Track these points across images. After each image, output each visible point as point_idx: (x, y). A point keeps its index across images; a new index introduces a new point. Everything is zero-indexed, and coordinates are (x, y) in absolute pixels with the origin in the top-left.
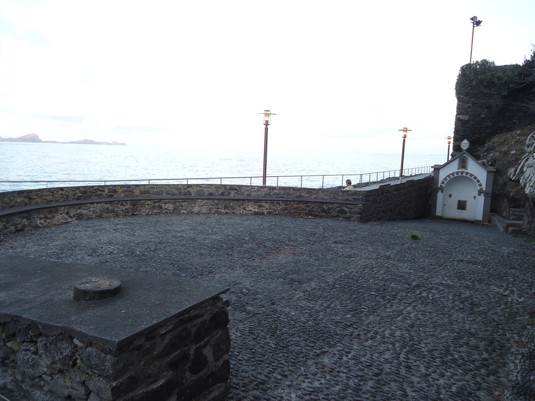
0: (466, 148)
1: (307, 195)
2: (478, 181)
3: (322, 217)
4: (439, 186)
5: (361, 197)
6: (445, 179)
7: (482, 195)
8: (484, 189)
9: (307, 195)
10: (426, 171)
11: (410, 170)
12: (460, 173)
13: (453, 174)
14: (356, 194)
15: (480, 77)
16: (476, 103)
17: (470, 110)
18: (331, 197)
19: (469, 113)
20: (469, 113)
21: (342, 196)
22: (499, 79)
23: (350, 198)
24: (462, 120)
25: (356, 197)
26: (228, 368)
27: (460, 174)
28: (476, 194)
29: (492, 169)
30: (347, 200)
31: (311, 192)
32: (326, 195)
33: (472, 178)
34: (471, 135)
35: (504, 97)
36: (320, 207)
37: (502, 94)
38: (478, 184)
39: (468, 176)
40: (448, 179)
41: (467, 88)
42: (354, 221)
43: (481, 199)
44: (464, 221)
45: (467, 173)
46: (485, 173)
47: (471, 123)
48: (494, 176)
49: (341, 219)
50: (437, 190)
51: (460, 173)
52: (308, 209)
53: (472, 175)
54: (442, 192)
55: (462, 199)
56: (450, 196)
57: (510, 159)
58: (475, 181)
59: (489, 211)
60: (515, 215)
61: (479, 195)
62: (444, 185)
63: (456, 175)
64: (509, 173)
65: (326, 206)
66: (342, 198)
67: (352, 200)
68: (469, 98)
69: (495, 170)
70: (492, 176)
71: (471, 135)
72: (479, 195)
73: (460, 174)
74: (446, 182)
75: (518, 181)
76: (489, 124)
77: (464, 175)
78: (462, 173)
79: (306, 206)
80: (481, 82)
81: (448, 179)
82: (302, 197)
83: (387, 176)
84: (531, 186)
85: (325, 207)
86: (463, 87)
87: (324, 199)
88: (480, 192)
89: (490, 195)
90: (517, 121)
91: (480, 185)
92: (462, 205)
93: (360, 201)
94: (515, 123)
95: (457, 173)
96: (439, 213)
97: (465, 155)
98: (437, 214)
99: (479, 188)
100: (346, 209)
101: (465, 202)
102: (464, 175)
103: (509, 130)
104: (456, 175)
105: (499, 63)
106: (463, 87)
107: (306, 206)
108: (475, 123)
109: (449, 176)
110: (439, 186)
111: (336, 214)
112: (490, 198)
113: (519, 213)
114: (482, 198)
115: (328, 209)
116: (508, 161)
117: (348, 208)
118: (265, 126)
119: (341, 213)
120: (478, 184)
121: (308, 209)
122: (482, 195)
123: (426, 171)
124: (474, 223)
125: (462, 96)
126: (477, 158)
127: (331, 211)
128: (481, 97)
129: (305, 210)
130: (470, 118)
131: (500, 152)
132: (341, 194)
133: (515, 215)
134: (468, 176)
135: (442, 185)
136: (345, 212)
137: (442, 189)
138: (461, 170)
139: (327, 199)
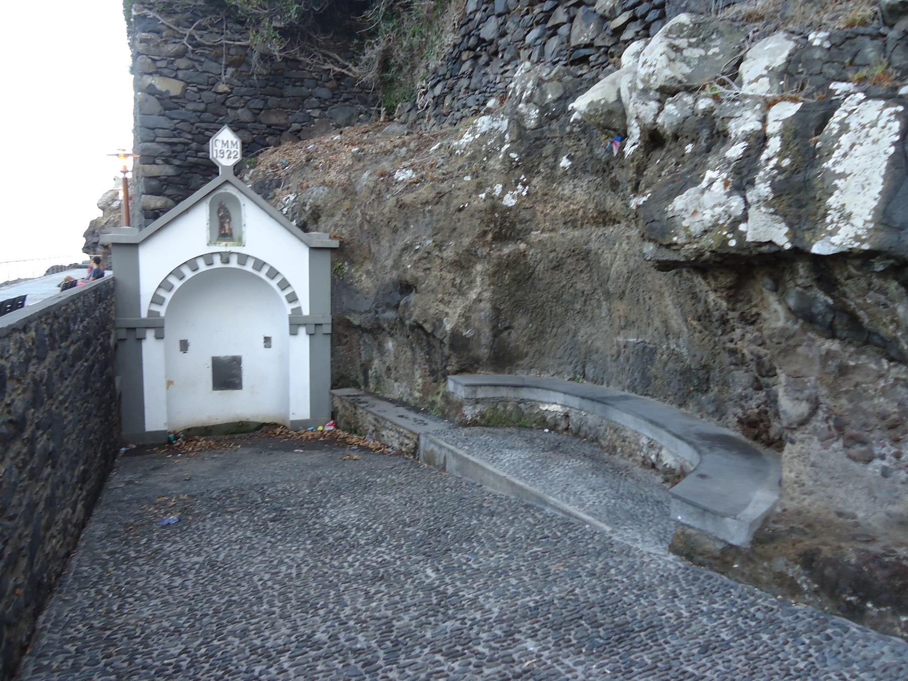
0: (231, 162)
2: (284, 285)
4: (144, 314)
6: (165, 285)
7: (302, 331)
8: (306, 312)
13: (192, 264)
17: (182, 63)
19: (181, 74)
20: (181, 74)
24: (161, 93)
28: (279, 328)
29: (321, 238)
33: (262, 274)
38: (283, 295)
39: (249, 267)
40: (177, 284)
45: (243, 259)
46: (302, 255)
47: (190, 106)
48: (333, 264)
50: (136, 333)
53: (259, 264)
54: (159, 337)
55: (226, 351)
56: (184, 346)
57: (408, 198)
58: (274, 283)
59: (329, 385)
60: (477, 401)
61: (293, 333)
62: (162, 310)
63: (203, 267)
69: (335, 244)
70: (326, 260)
72: (293, 333)
73: (218, 263)
74: (168, 296)
77: (234, 263)
81: (177, 284)
89: (328, 329)
90: (316, 113)
91: (292, 298)
92: (227, 374)
94: (311, 118)
95: (208, 258)
99: (289, 308)
101: (236, 362)
103: (297, 136)
108: (202, 107)
109: (177, 272)
110: (144, 314)
112: (329, 338)
113: (490, 393)
114: (303, 341)
116: (402, 206)
120: (283, 295)
122: (302, 331)
126: (266, 191)
128: (212, 25)
130: (185, 90)
133: (477, 401)
134: (249, 267)
135: (155, 308)
137: (158, 327)
138: (222, 247)
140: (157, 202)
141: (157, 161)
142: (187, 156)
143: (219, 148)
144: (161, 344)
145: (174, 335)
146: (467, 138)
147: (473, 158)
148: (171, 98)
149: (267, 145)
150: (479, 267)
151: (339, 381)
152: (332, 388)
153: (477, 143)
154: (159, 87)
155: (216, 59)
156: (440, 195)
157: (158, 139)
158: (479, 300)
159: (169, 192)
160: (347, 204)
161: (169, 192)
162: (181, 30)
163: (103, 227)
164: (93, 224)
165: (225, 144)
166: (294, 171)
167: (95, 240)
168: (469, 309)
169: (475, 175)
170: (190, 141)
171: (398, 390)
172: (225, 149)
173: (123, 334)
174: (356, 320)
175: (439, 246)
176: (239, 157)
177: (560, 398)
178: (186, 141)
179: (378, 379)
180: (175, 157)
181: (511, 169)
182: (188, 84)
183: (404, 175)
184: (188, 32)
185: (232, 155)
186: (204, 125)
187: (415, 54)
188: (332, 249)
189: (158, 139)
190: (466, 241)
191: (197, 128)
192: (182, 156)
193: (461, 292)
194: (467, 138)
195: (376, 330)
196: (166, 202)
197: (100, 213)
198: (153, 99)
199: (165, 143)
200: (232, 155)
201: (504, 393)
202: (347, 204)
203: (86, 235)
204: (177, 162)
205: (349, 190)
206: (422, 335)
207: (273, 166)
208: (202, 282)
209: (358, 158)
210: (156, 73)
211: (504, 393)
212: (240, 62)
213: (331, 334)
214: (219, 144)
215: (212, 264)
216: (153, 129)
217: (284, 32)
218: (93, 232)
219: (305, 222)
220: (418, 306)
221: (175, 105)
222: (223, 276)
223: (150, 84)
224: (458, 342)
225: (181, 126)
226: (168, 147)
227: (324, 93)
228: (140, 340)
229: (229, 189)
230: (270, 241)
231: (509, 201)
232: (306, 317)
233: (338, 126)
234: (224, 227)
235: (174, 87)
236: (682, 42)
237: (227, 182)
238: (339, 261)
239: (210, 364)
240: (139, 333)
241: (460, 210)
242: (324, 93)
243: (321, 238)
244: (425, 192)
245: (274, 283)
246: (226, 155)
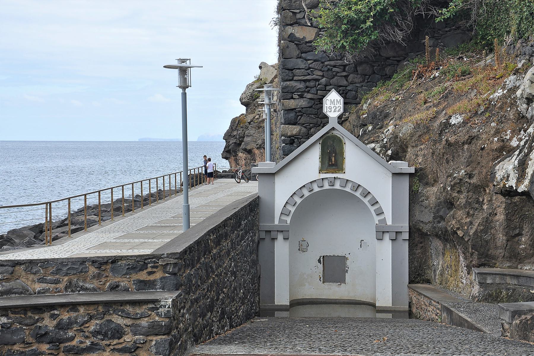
8: (389, 222)
10: (167, 185)
11: (146, 185)
14: (144, 267)
21: (98, 277)
24: (299, 40)
25: (143, 276)
27: (327, 186)
28: (370, 236)
33: (358, 194)
39: (348, 189)
50: (271, 235)
58: (372, 209)
64: (499, 175)
69: (412, 170)
74: (293, 209)
83: (77, 205)
85: (48, 323)
91: (380, 213)
92: (334, 268)
96: (282, 298)
98: (276, 303)
99: (377, 219)
101: (343, 259)
102: (337, 186)
110: (277, 222)
111: (88, 343)
112: (407, 244)
114: (387, 245)
115: (60, 326)
117: (128, 316)
118: (181, 91)
122: (387, 237)
123: (167, 185)
140: (294, 130)
141: (294, 96)
142: (317, 90)
143: (328, 106)
144: (287, 244)
148: (307, 42)
152: (409, 283)
154: (297, 35)
157: (295, 78)
165: (332, 102)
169: (500, 122)
170: (320, 77)
172: (332, 106)
173: (263, 235)
176: (342, 111)
178: (317, 77)
180: (308, 92)
181: (518, 119)
185: (337, 110)
186: (332, 63)
188: (411, 175)
189: (295, 78)
191: (327, 65)
192: (313, 90)
196: (300, 130)
199: (300, 80)
200: (337, 110)
204: (309, 96)
210: (296, 23)
213: (409, 240)
214: (328, 103)
215: (333, 185)
216: (292, 70)
221: (310, 49)
223: (291, 34)
226: (303, 83)
228: (274, 239)
230: (361, 166)
232: (390, 226)
234: (332, 159)
237: (333, 129)
240: (273, 234)
241: (482, 149)
246: (333, 110)
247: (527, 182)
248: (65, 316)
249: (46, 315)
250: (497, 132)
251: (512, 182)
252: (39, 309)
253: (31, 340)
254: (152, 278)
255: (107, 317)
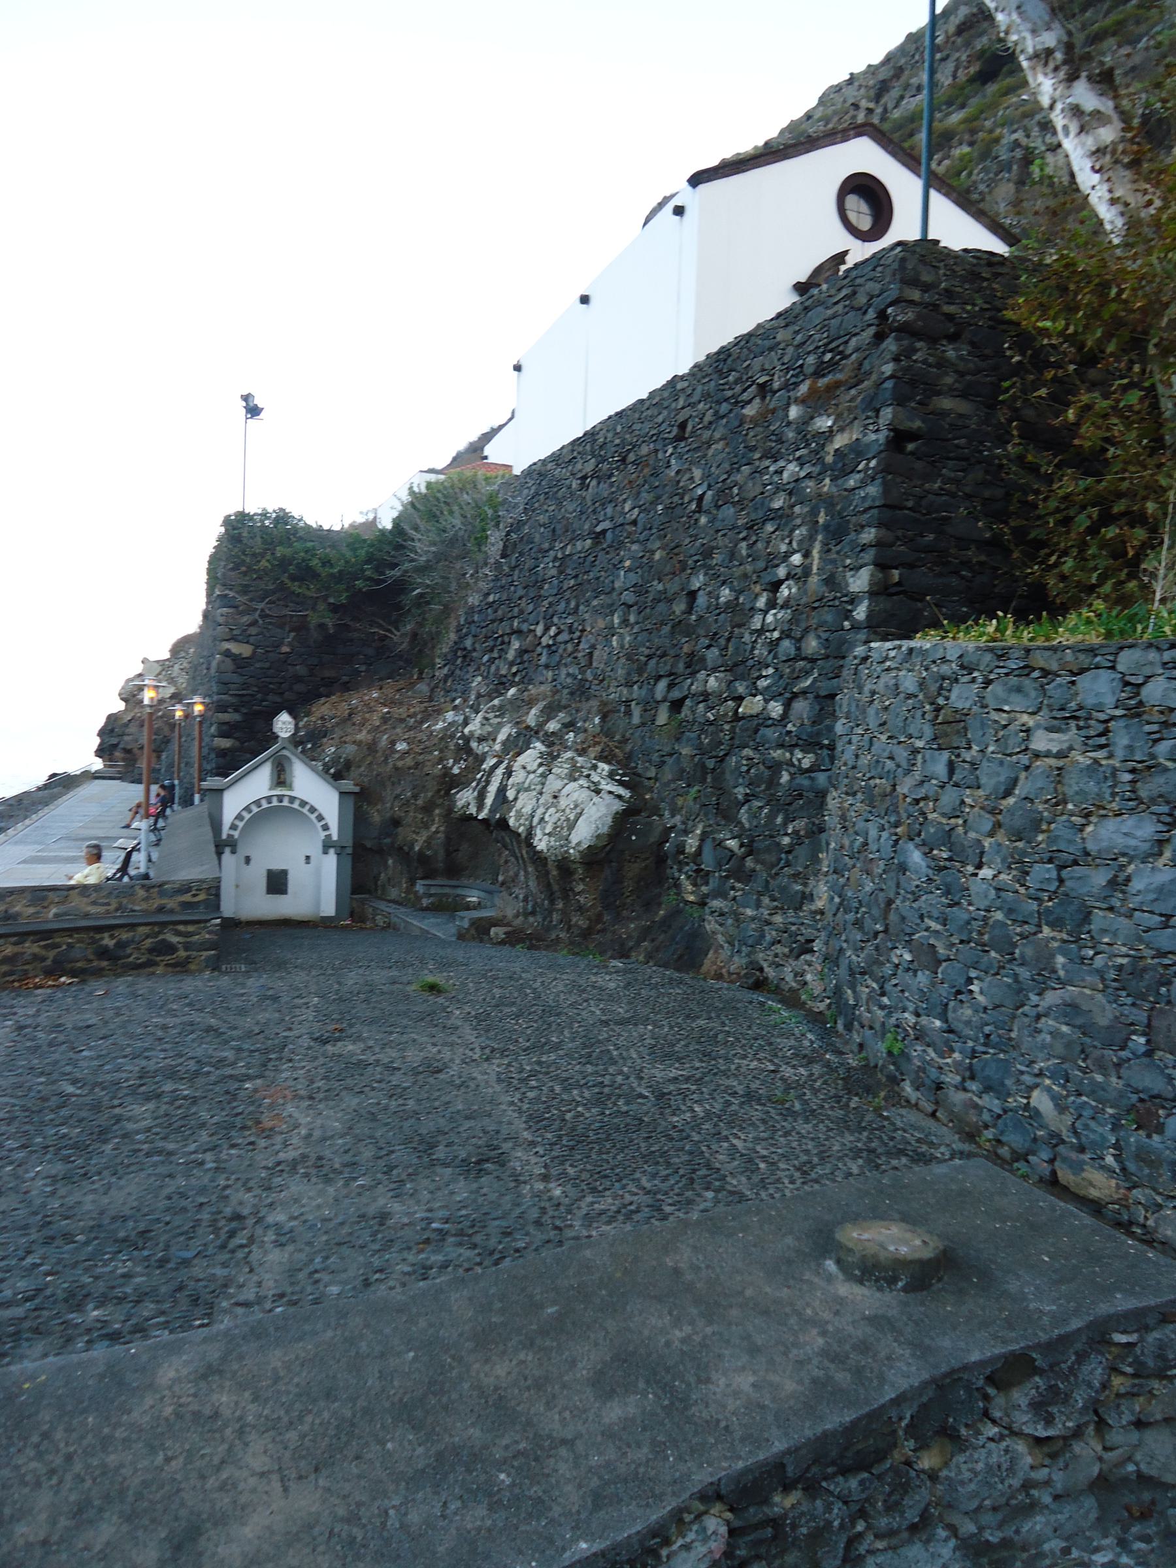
0: (288, 735)
1: (31, 910)
2: (320, 818)
3: (98, 973)
4: (224, 836)
5: (202, 897)
6: (239, 817)
7: (332, 851)
8: (335, 837)
9: (31, 910)
12: (275, 800)
13: (257, 803)
14: (189, 890)
15: (280, 551)
16: (268, 616)
17: (253, 630)
18: (112, 908)
19: (252, 639)
20: (252, 639)
21: (146, 899)
22: (327, 562)
23: (171, 904)
25: (187, 898)
26: (876, 1316)
27: (275, 803)
28: (315, 849)
29: (348, 785)
30: (161, 909)
31: (44, 899)
32: (94, 903)
33: (305, 810)
34: (259, 696)
35: (335, 609)
36: (94, 941)
37: (332, 600)
39: (296, 805)
41: (245, 574)
42: (201, 971)
43: (330, 863)
44: (286, 923)
45: (292, 799)
49: (159, 970)
51: (275, 800)
52: (51, 954)
53: (303, 803)
54: (233, 852)
55: (277, 866)
56: (248, 860)
57: (400, 764)
58: (313, 817)
60: (431, 895)
61: (325, 852)
62: (236, 834)
64: (460, 804)
65: (112, 937)
66: (144, 906)
67: (178, 909)
68: (251, 600)
69: (357, 789)
71: (259, 696)
73: (275, 803)
74: (241, 824)
75: (503, 824)
76: (301, 670)
77: (286, 803)
78: (280, 798)
79: (45, 947)
80: (284, 563)
82: (15, 917)
84: (549, 834)
85: (108, 941)
86: (232, 569)
87: (87, 916)
88: (327, 846)
89: (349, 850)
90: (363, 668)
91: (326, 828)
92: (277, 883)
93: (202, 909)
95: (269, 799)
97: (285, 752)
99: (323, 834)
100: (175, 939)
101: (284, 873)
102: (286, 803)
103: (347, 687)
104: (265, 805)
105: (312, 520)
106: (232, 569)
107: (45, 947)
108: (267, 665)
109: (247, 809)
110: (224, 836)
112: (349, 858)
116: (396, 769)
117: (178, 933)
119: (160, 954)
121: (51, 954)
122: (332, 851)
124: (324, 924)
125: (232, 594)
126: (310, 757)
127: (129, 951)
129: (44, 959)
130: (254, 652)
131: (358, 743)
132: (141, 893)
133: (431, 895)
136: (171, 949)
139: (97, 917)
145: (243, 851)
146: (440, 725)
147: (442, 739)
149: (320, 696)
150: (437, 811)
151: (355, 891)
153: (445, 729)
155: (281, 626)
156: (417, 764)
158: (437, 832)
159: (237, 735)
160: (369, 759)
161: (237, 735)
162: (254, 605)
163: (126, 725)
164: (112, 719)
166: (338, 724)
167: (114, 741)
168: (430, 838)
169: (441, 751)
171: (394, 893)
174: (369, 844)
175: (415, 797)
177: (476, 893)
179: (383, 886)
182: (257, 647)
183: (401, 746)
184: (261, 606)
187: (435, 638)
190: (430, 794)
193: (427, 827)
194: (440, 725)
195: (380, 852)
197: (121, 706)
198: (228, 660)
201: (447, 890)
202: (369, 759)
203: (101, 733)
204: (245, 711)
205: (372, 747)
206: (403, 853)
207: (322, 718)
208: (263, 815)
209: (385, 719)
211: (447, 890)
212: (301, 627)
217: (335, 609)
218: (112, 731)
219: (336, 773)
220: (404, 834)
222: (276, 813)
224: (422, 859)
225: (251, 680)
227: (370, 651)
229: (285, 752)
230: (312, 788)
231: (456, 771)
233: (381, 679)
234: (281, 778)
235: (244, 650)
236: (491, 715)
238: (359, 802)
239: (265, 874)
242: (370, 651)
243: (348, 785)
244: (409, 761)
245: (313, 817)
247: (486, 811)
248: (125, 936)
249: (106, 935)
250: (441, 760)
251: (473, 810)
252: (100, 929)
253: (91, 957)
254: (196, 899)
255: (161, 937)
